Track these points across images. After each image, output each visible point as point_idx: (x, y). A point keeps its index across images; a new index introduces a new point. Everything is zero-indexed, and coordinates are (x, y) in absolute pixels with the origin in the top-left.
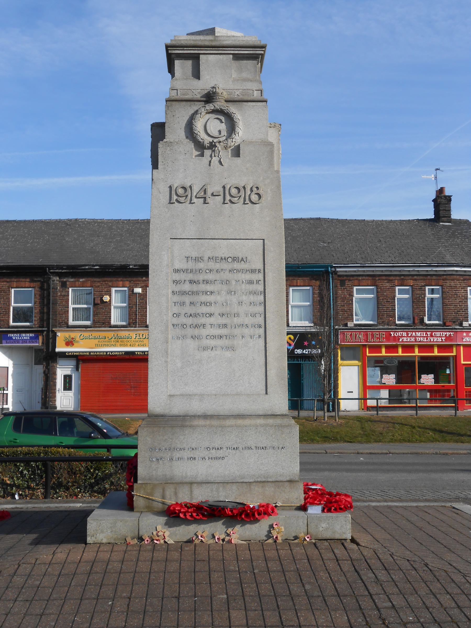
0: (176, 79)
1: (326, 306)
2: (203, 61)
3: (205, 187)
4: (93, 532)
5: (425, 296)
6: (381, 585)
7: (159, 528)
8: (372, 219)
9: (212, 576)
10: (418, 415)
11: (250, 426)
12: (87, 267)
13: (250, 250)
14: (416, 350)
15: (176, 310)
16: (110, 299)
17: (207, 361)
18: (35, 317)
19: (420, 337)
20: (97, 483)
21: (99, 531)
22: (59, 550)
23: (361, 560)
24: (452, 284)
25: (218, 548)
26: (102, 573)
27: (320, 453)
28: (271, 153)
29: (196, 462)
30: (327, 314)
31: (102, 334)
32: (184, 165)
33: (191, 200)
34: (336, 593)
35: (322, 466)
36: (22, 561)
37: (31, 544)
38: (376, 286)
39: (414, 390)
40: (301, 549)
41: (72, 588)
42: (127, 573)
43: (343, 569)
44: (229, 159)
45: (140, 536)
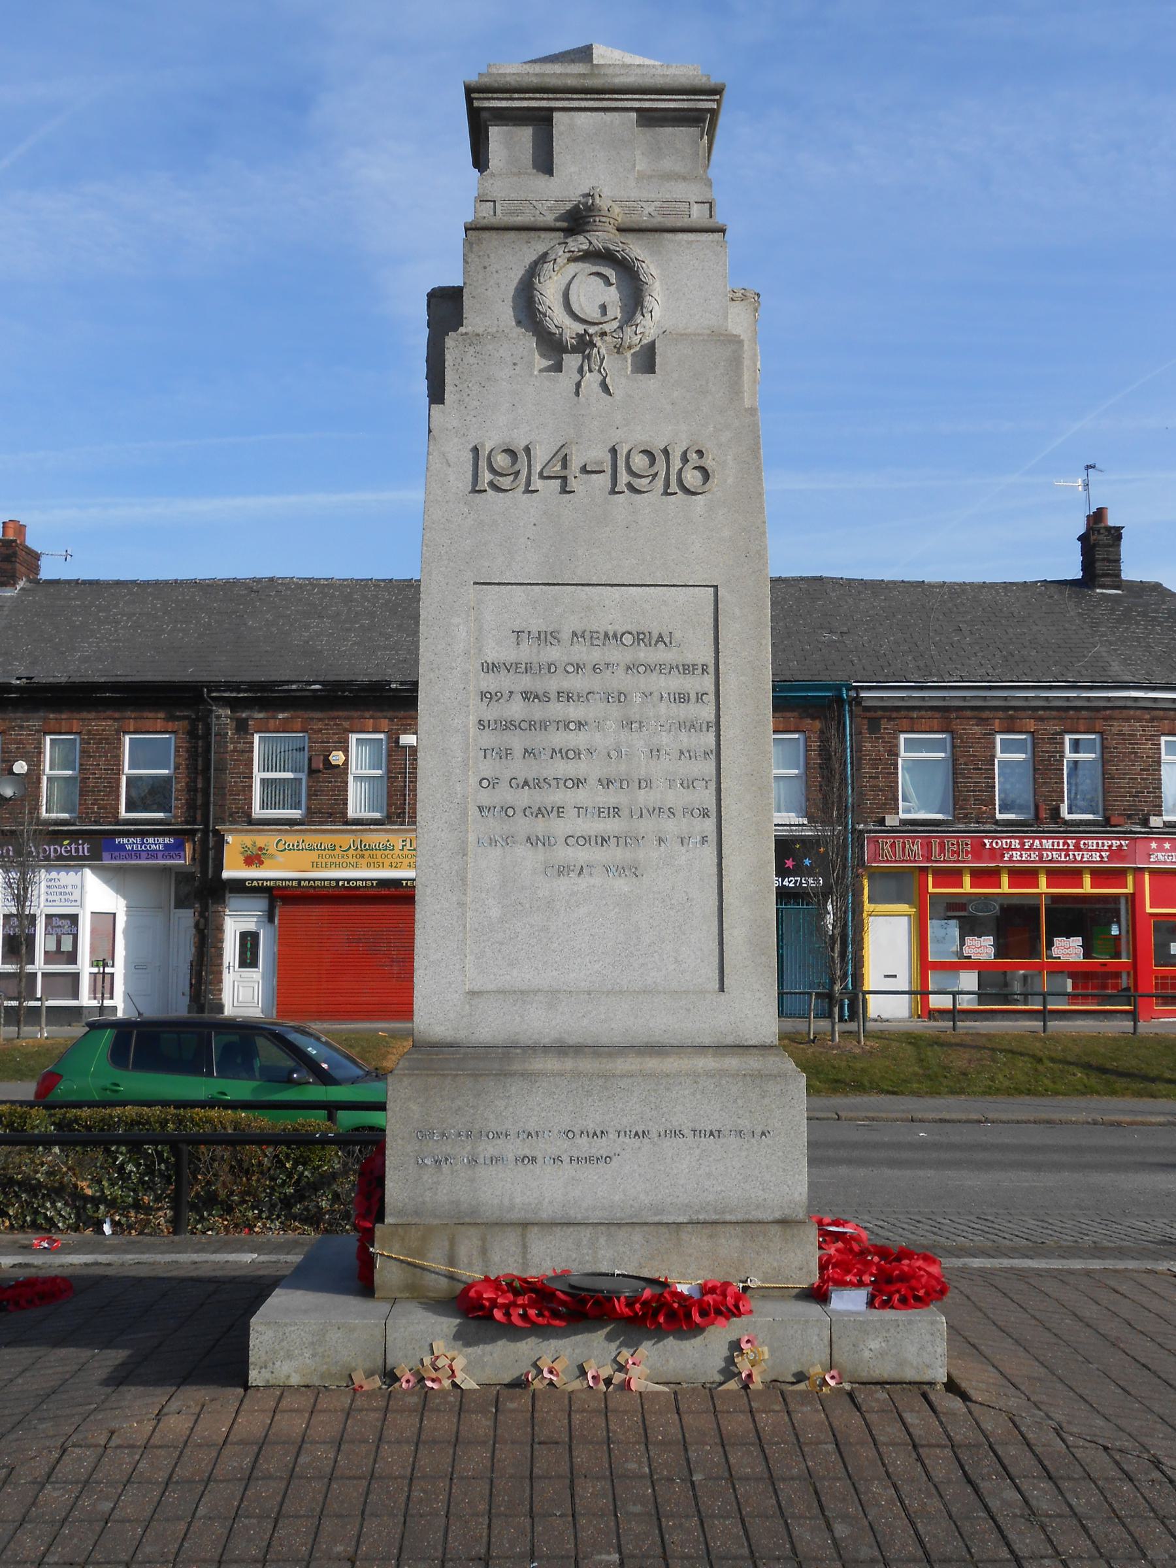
0: (493, 175)
1: (837, 776)
2: (562, 128)
3: (564, 451)
4: (264, 1358)
5: (1063, 756)
6: (1043, 1528)
7: (439, 1346)
8: (940, 579)
9: (578, 1489)
10: (1049, 1030)
11: (678, 1074)
12: (294, 687)
13: (681, 614)
14: (1043, 880)
15: (487, 768)
16: (347, 760)
17: (567, 902)
18: (177, 799)
19: (1051, 850)
20: (300, 1196)
21: (282, 1353)
22: (174, 1405)
23: (978, 1446)
24: (1126, 729)
25: (594, 1405)
26: (281, 1478)
27: (824, 1119)
28: (736, 362)
29: (537, 1168)
30: (840, 797)
31: (327, 839)
32: (510, 394)
33: (528, 482)
34: (920, 1553)
35: (831, 1153)
36: (74, 1439)
37: (106, 1382)
38: (952, 732)
39: (1036, 972)
40: (817, 1411)
41: (197, 1524)
42: (349, 1478)
43: (933, 1474)
44: (628, 377)
45: (388, 1367)
